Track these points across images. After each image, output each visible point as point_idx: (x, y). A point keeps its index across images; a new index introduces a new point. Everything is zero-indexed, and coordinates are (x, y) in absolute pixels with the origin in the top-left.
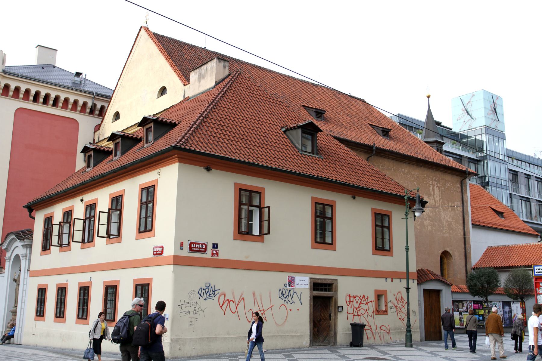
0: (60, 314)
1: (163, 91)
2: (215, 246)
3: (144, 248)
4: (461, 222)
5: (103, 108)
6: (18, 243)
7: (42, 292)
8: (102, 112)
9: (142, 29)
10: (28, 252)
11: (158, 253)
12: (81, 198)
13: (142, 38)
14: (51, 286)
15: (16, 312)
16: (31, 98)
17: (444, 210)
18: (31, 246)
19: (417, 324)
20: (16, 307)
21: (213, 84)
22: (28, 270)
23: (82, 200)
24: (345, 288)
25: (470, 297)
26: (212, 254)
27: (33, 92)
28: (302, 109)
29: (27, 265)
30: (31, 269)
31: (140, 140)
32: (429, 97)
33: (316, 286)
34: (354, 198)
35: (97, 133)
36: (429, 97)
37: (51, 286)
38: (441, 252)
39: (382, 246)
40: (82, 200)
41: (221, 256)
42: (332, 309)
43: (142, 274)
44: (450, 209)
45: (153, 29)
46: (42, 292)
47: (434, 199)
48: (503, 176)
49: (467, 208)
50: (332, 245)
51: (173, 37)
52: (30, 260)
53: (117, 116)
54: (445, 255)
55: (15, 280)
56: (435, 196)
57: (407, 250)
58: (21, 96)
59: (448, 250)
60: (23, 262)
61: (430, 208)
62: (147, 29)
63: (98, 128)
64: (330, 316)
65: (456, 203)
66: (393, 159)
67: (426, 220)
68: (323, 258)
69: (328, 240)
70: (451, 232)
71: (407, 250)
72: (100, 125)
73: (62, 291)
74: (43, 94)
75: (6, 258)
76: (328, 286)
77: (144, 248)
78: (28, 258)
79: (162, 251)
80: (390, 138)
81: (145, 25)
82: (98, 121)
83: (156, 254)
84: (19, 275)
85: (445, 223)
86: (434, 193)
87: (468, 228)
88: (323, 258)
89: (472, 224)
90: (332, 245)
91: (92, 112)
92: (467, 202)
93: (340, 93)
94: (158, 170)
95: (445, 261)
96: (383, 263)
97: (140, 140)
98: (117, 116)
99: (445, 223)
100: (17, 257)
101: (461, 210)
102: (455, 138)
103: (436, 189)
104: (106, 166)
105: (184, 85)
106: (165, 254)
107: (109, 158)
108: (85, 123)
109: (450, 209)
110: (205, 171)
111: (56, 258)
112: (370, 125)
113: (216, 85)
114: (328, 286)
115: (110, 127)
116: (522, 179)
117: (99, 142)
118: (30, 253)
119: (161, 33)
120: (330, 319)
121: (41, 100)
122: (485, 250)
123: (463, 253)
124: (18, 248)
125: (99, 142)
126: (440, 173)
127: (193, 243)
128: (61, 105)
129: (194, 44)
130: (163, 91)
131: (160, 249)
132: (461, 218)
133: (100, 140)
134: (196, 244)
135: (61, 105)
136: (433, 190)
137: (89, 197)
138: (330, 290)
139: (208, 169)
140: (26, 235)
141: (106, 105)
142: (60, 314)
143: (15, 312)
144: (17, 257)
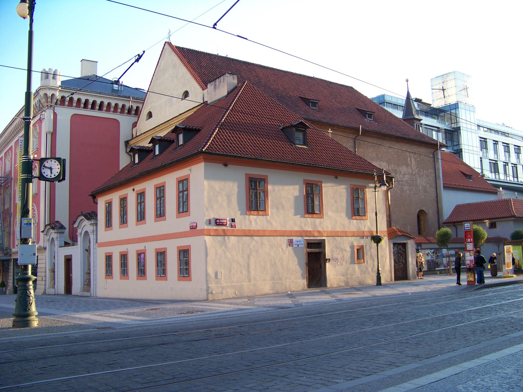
0: (124, 272)
1: (186, 94)
2: (233, 220)
3: (183, 224)
4: (434, 186)
5: (138, 108)
6: (86, 222)
7: (109, 258)
8: (137, 112)
9: (166, 44)
10: (95, 229)
11: (193, 228)
12: (132, 188)
13: (167, 51)
14: (116, 252)
15: (90, 273)
16: (82, 105)
17: (419, 177)
18: (96, 224)
19: (387, 268)
20: (90, 269)
21: (226, 93)
22: (96, 242)
23: (133, 190)
26: (232, 226)
27: (83, 101)
28: (300, 99)
29: (95, 238)
30: (98, 242)
31: (173, 141)
32: (407, 81)
34: (336, 178)
35: (135, 128)
36: (407, 81)
37: (116, 252)
38: (418, 211)
40: (133, 190)
41: (238, 227)
42: (322, 261)
43: (184, 242)
44: (425, 176)
45: (174, 44)
46: (109, 258)
47: (412, 168)
48: (475, 145)
49: (439, 172)
51: (191, 48)
52: (97, 235)
53: (150, 115)
54: (421, 214)
55: (87, 250)
56: (412, 166)
58: (75, 104)
59: (424, 209)
60: (92, 237)
61: (408, 176)
62: (170, 44)
63: (135, 125)
64: (321, 266)
65: (430, 171)
66: (376, 138)
67: (405, 186)
68: (309, 224)
70: (426, 194)
72: (136, 123)
73: (124, 257)
74: (91, 101)
75: (78, 234)
76: (320, 244)
77: (183, 224)
78: (95, 233)
79: (196, 226)
81: (168, 40)
82: (135, 119)
83: (192, 228)
84: (90, 246)
85: (421, 187)
86: (411, 163)
87: (440, 190)
88: (309, 224)
89: (444, 187)
91: (129, 112)
92: (439, 169)
94: (189, 168)
95: (422, 218)
96: (354, 225)
97: (173, 141)
98: (150, 115)
99: (421, 187)
100: (86, 233)
101: (434, 176)
103: (413, 160)
104: (149, 164)
105: (203, 90)
106: (198, 228)
107: (150, 155)
108: (125, 121)
109: (425, 176)
110: (224, 166)
111: (117, 232)
113: (228, 94)
115: (145, 125)
116: (490, 145)
117: (137, 136)
118: (97, 230)
119: (181, 46)
120: (321, 268)
121: (90, 106)
122: (454, 207)
123: (436, 211)
124: (86, 225)
125: (137, 136)
126: (416, 147)
127: (218, 219)
128: (105, 109)
129: (208, 52)
130: (186, 94)
131: (195, 225)
132: (434, 182)
133: (138, 135)
134: (220, 220)
135: (105, 109)
136: (411, 160)
137: (139, 187)
138: (320, 247)
139: (226, 165)
140: (92, 216)
141: (140, 106)
142: (124, 272)
143: (89, 273)
144: (86, 233)
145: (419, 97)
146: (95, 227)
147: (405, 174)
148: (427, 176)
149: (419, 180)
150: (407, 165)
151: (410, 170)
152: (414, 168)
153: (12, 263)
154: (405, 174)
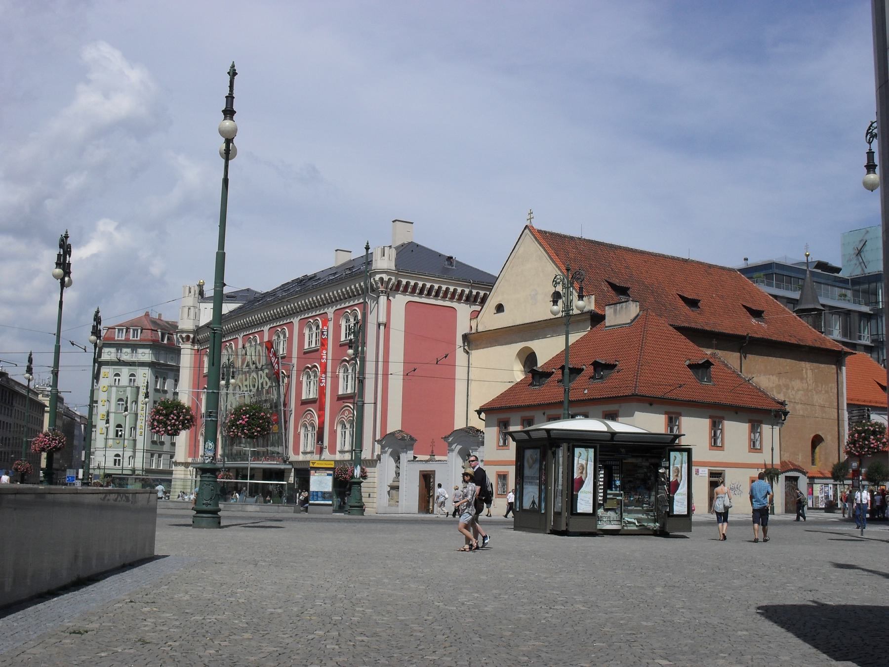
17: (817, 393)
24: (730, 475)
25: (832, 481)
33: (712, 474)
38: (812, 436)
39: (754, 447)
45: (537, 225)
50: (721, 448)
57: (772, 450)
69: (719, 444)
71: (772, 450)
76: (719, 474)
80: (763, 320)
81: (528, 223)
88: (717, 456)
90: (721, 448)
91: (468, 300)
93: (710, 266)
98: (500, 308)
102: (844, 285)
103: (809, 372)
112: (744, 306)
114: (719, 474)
136: (806, 373)
139: (651, 405)
145: (824, 259)
146: (816, 481)
147: (798, 390)
148: (827, 392)
149: (816, 397)
150: (802, 379)
151: (805, 386)
152: (810, 382)
153: (292, 474)
154: (798, 390)
